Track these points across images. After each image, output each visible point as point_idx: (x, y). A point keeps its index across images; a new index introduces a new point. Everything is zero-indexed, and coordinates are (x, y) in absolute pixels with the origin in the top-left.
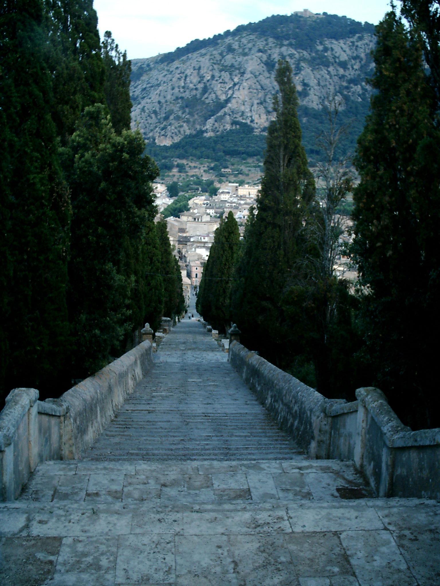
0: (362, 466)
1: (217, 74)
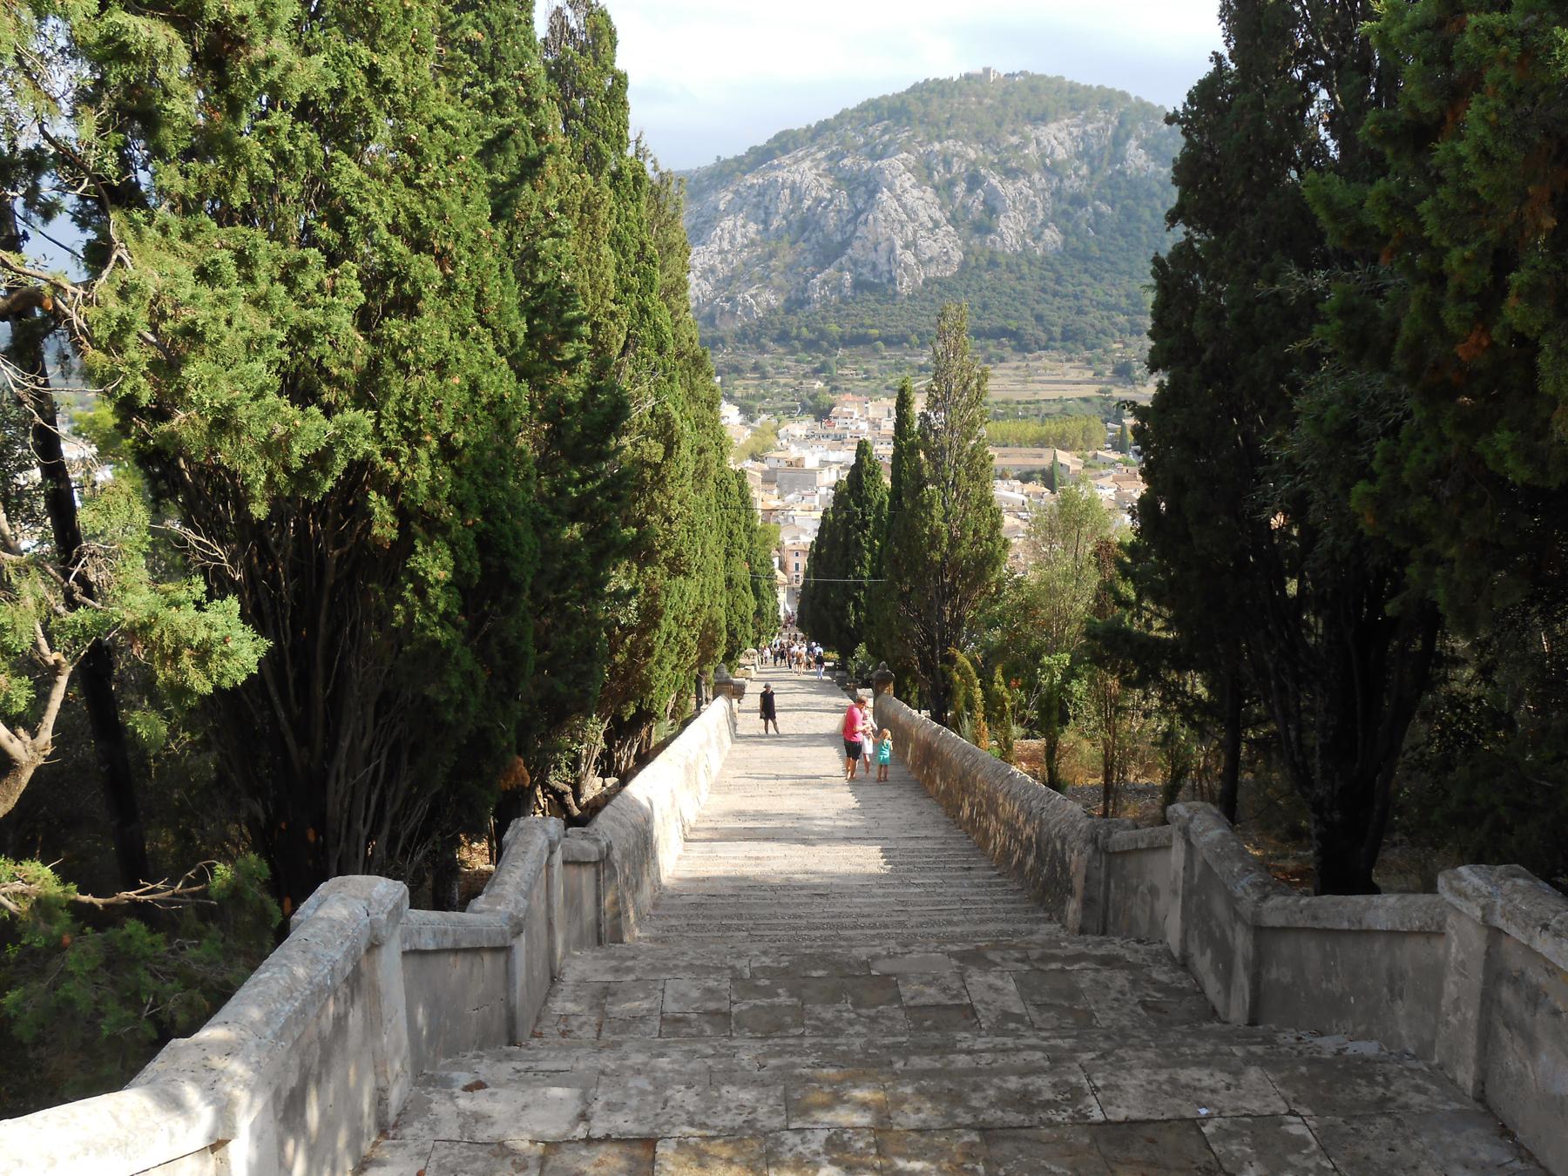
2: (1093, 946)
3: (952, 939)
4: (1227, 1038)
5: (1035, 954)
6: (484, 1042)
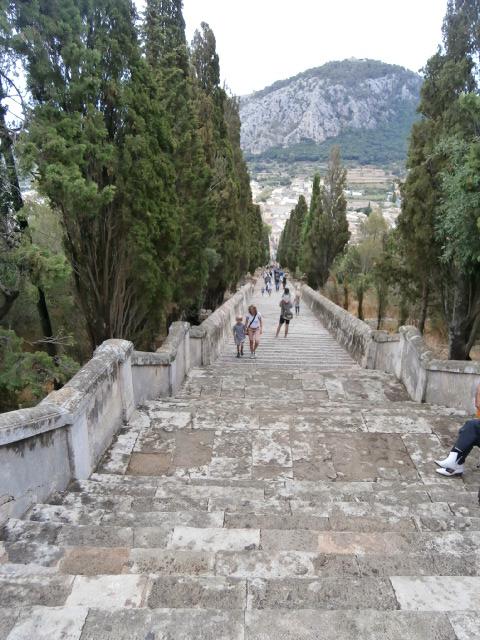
0: (401, 376)
1: (292, 105)
2: (370, 373)
3: (322, 368)
4: (413, 406)
5: (350, 375)
6: (160, 396)
